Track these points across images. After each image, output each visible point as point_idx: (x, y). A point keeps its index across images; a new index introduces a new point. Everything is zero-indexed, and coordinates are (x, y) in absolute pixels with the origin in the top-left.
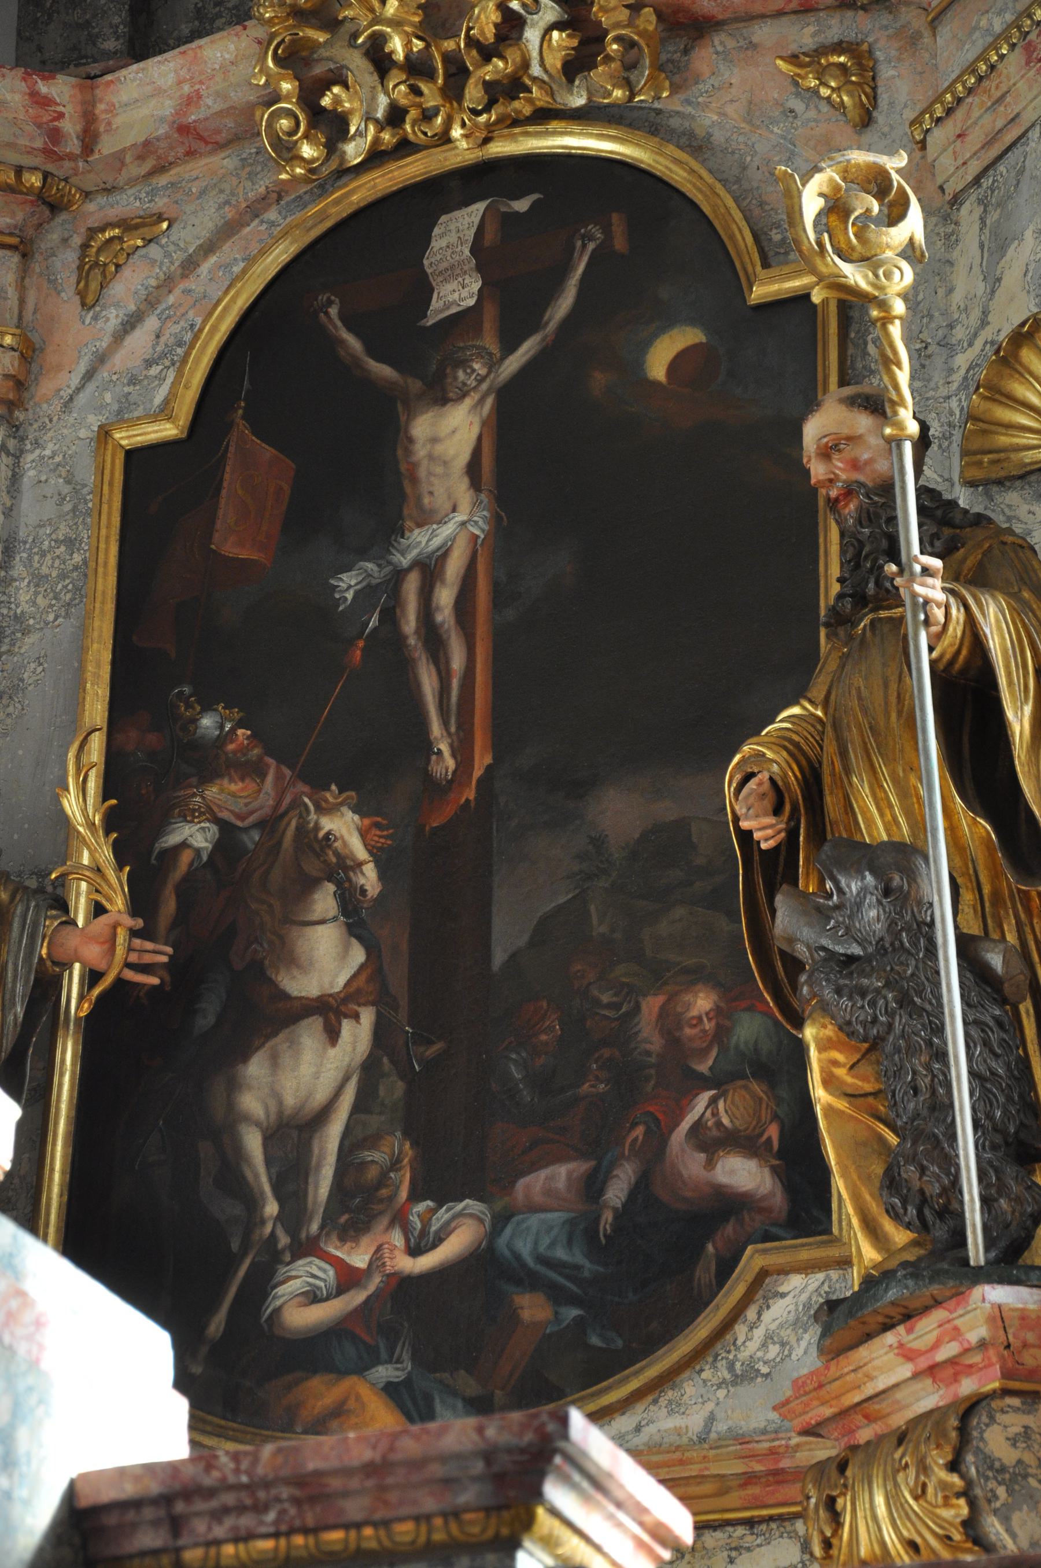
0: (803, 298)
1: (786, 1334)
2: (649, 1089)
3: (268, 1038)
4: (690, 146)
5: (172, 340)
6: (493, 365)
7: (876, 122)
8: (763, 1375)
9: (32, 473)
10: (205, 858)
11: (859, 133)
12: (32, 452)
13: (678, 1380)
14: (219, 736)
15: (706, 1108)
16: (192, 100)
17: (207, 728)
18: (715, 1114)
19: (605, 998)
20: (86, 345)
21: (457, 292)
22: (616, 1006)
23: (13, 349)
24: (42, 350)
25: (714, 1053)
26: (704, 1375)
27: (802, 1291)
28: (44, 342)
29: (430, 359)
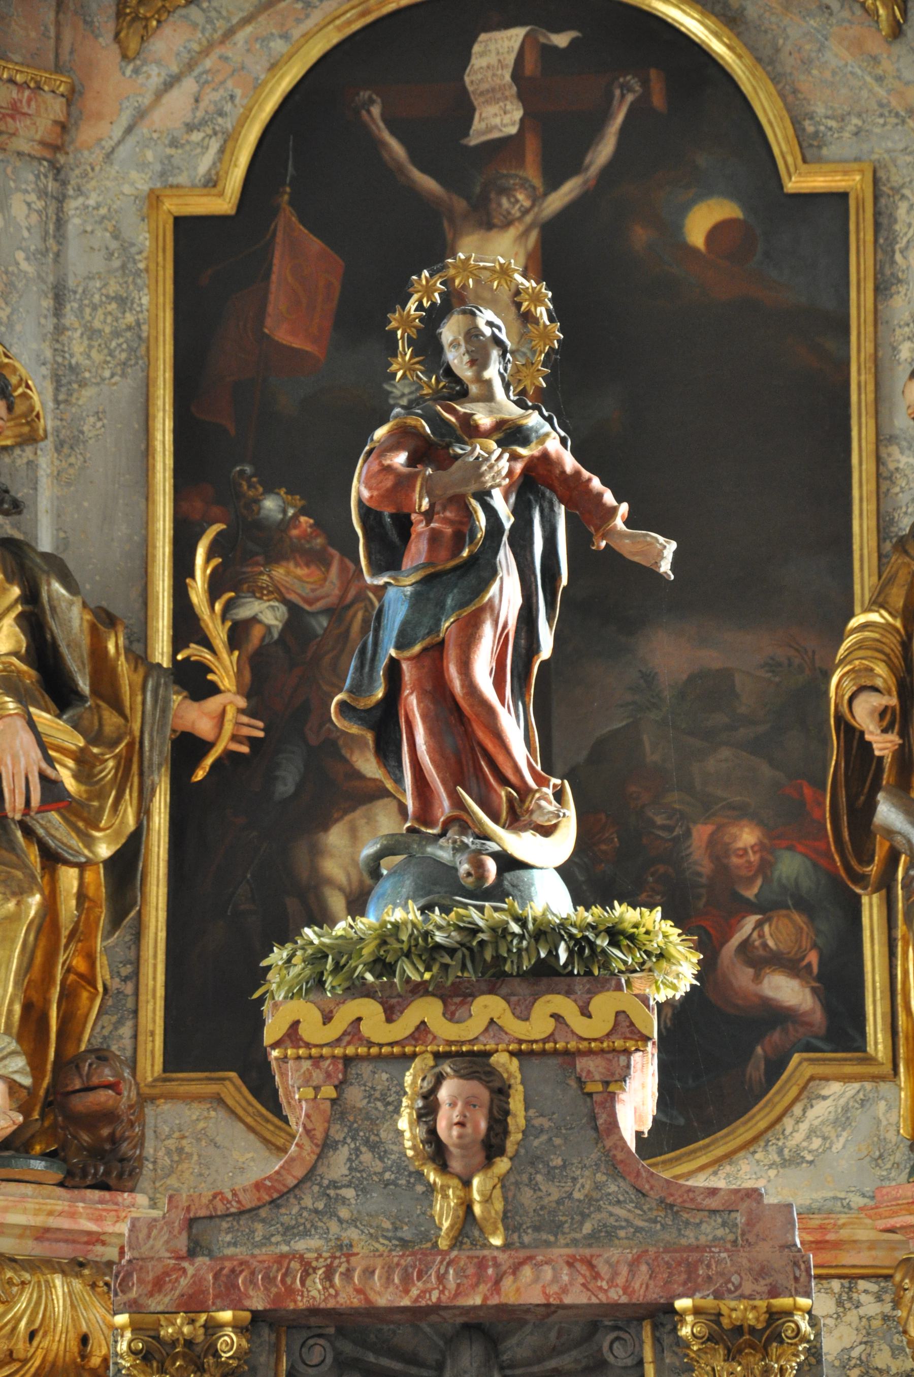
0: (843, 196)
1: (827, 1130)
2: (701, 904)
3: (346, 812)
4: (724, 15)
5: (212, 108)
6: (537, 199)
7: (905, 35)
8: (808, 1162)
9: (76, 221)
10: (276, 635)
11: (890, 43)
12: (76, 198)
13: (735, 1157)
14: (282, 520)
15: (754, 929)
17: (270, 510)
18: (761, 936)
19: (659, 820)
20: (127, 98)
21: (498, 118)
22: (670, 829)
23: (63, 95)
24: (81, 94)
25: (759, 882)
26: (757, 1156)
27: (841, 1096)
28: (83, 86)
29: (477, 179)
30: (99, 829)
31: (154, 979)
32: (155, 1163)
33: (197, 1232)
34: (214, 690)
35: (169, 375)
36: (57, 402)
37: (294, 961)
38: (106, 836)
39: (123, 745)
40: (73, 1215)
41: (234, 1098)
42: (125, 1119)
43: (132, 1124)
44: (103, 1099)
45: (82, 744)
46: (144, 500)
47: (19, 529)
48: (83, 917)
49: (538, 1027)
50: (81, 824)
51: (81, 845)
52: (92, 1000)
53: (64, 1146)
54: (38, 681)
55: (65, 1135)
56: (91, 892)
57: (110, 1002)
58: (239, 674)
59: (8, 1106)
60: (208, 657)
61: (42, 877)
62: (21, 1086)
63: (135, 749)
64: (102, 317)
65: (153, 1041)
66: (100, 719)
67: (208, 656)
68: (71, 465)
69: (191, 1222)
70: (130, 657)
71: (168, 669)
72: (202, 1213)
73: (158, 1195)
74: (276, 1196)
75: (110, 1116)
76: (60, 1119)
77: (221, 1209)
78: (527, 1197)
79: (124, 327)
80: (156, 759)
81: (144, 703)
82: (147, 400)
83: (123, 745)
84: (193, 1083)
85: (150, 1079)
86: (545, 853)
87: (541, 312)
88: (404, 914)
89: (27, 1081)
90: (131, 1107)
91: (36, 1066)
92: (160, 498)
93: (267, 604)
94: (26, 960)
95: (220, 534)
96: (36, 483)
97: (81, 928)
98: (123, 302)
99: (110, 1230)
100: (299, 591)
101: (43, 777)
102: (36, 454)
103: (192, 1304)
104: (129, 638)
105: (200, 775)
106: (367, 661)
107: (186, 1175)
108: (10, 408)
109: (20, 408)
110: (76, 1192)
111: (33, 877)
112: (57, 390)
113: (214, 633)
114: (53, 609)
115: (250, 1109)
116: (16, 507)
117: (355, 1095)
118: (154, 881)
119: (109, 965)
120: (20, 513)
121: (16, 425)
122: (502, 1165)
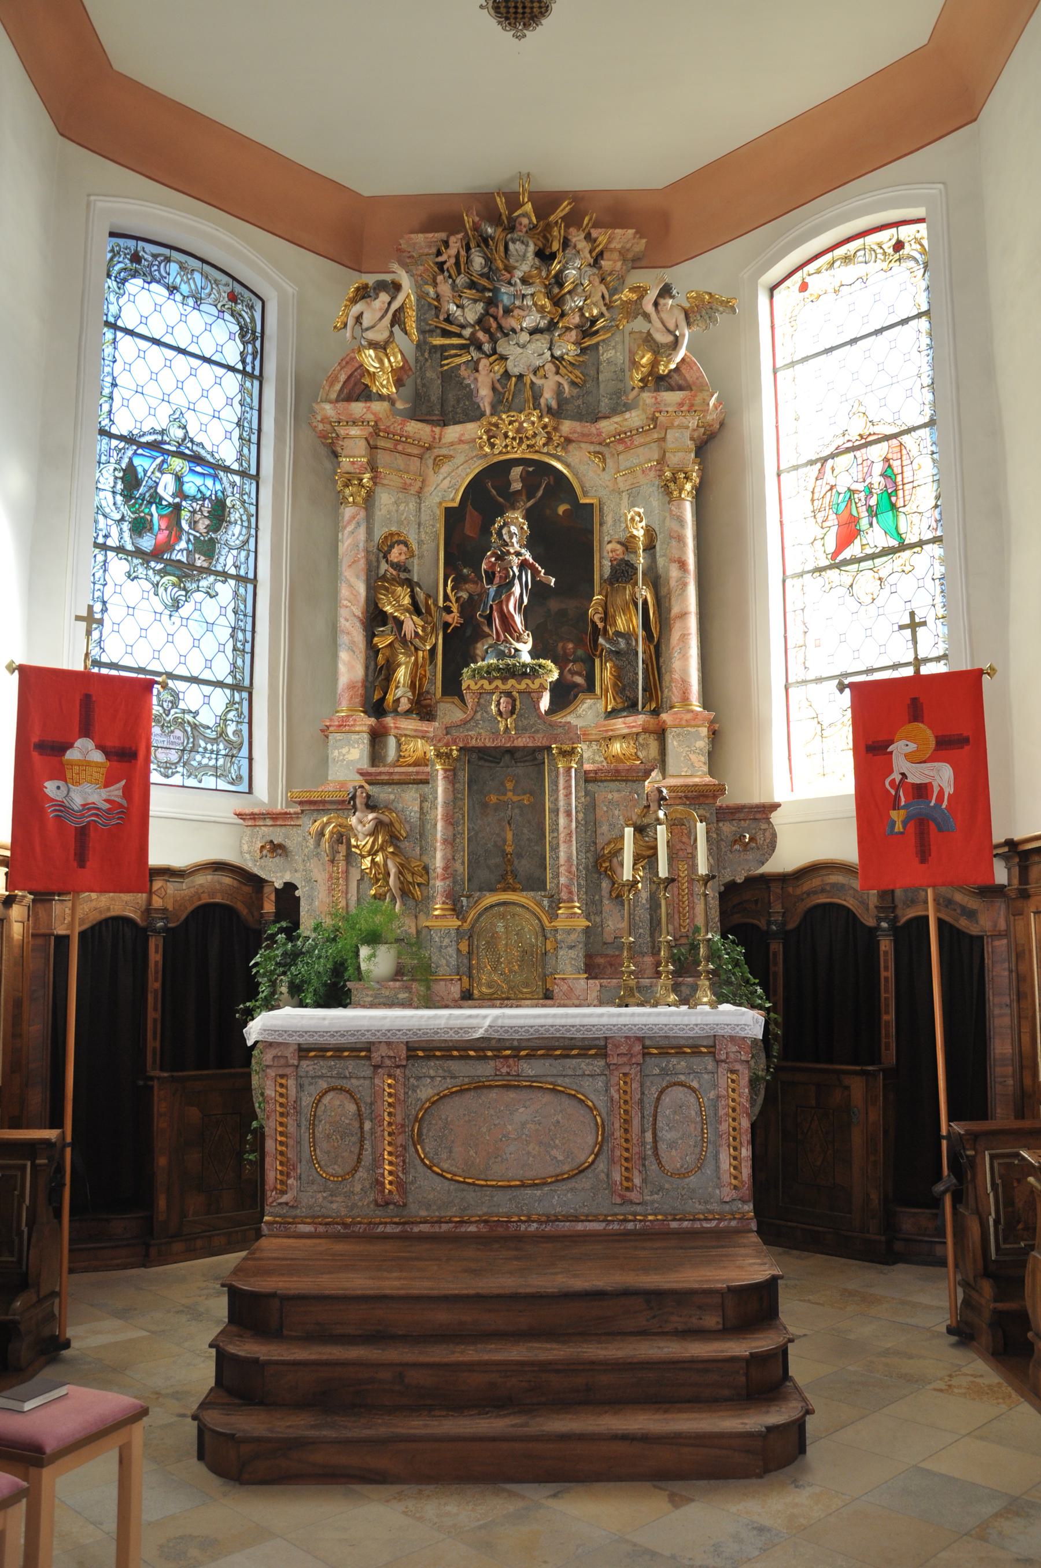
16: (463, 435)
21: (517, 486)
29: (511, 500)
33: (448, 730)
49: (522, 686)
74: (465, 723)
75: (430, 706)
78: (520, 723)
84: (448, 699)
86: (524, 649)
87: (525, 527)
88: (493, 661)
91: (414, 694)
98: (433, 526)
103: (447, 745)
106: (485, 605)
116: (409, 571)
117: (482, 701)
122: (515, 716)
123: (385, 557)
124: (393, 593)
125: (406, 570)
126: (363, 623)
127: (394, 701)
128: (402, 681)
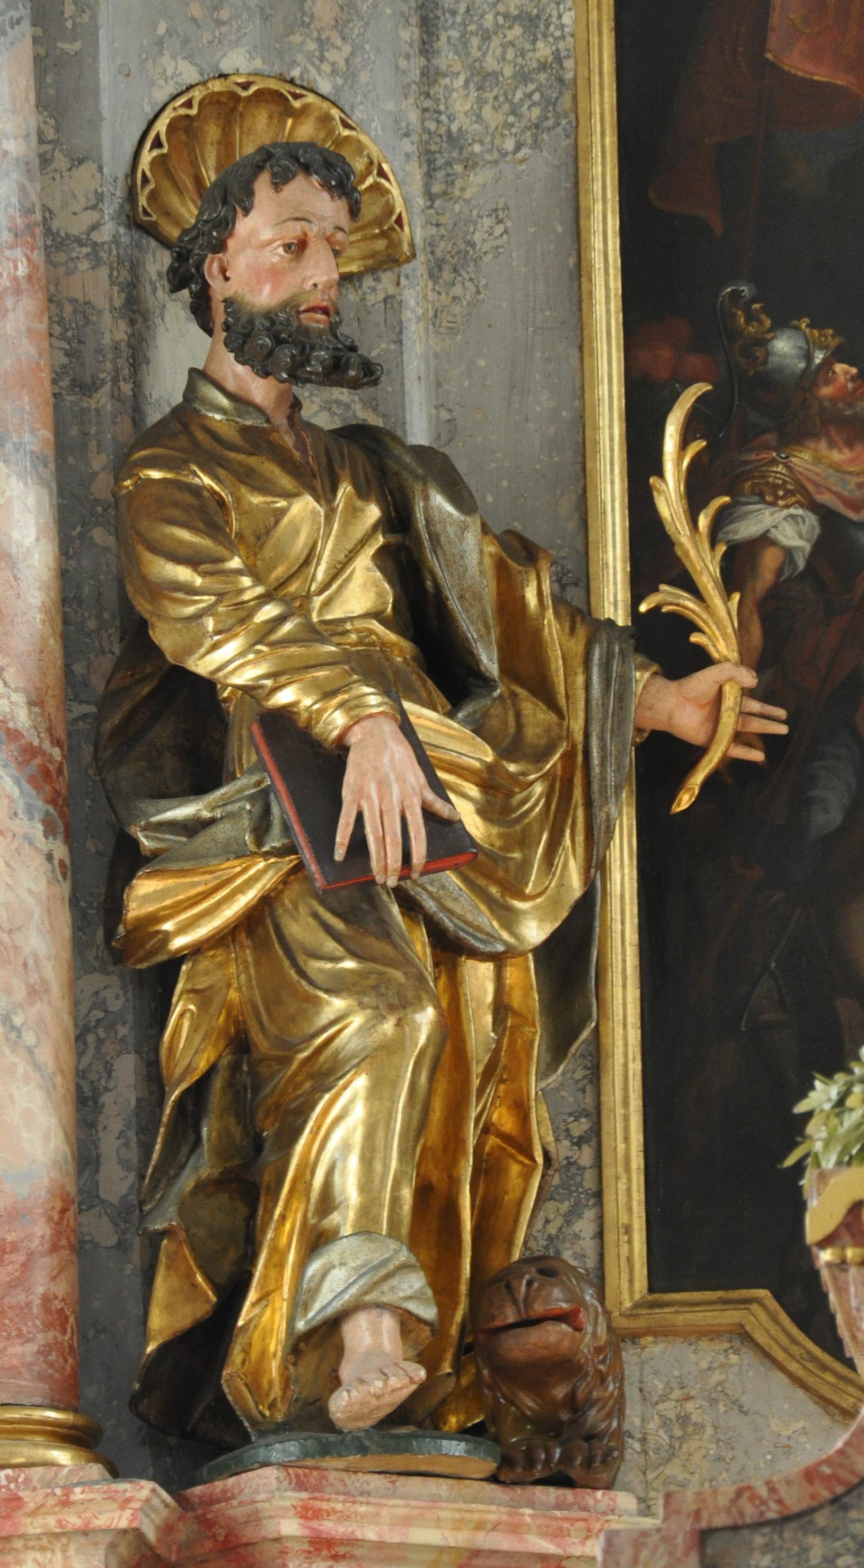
10: (801, 564)
14: (805, 371)
17: (785, 356)
30: (524, 897)
31: (626, 1139)
32: (643, 1440)
34: (701, 659)
35: (611, 140)
36: (430, 197)
37: (850, 1102)
38: (535, 908)
39: (557, 757)
40: (515, 1528)
41: (767, 1331)
42: (591, 1370)
43: (603, 1380)
44: (553, 1338)
45: (490, 757)
46: (576, 352)
47: (375, 409)
48: (505, 1041)
50: (494, 890)
51: (495, 924)
52: (527, 1177)
53: (494, 1416)
54: (414, 659)
55: (496, 1399)
56: (516, 1000)
57: (556, 1180)
58: (742, 631)
59: (401, 1356)
60: (691, 605)
61: (436, 979)
62: (419, 1320)
63: (578, 762)
64: (499, 52)
65: (630, 1242)
66: (518, 715)
67: (689, 603)
68: (455, 298)
69: (703, 1537)
70: (563, 611)
71: (625, 628)
72: (721, 1520)
73: (652, 1494)
75: (565, 1366)
76: (485, 1372)
77: (750, 1513)
79: (535, 65)
80: (611, 778)
81: (588, 686)
82: (576, 185)
83: (557, 757)
84: (697, 1308)
85: (628, 1304)
89: (429, 1312)
90: (598, 1350)
91: (443, 1289)
92: (601, 346)
93: (785, 512)
94: (416, 1114)
95: (702, 400)
96: (401, 332)
97: (503, 1060)
99: (577, 1551)
100: (838, 489)
101: (429, 815)
102: (398, 284)
104: (559, 580)
105: (685, 801)
107: (697, 1458)
108: (354, 211)
109: (370, 210)
110: (519, 1490)
111: (421, 979)
112: (429, 175)
113: (699, 566)
114: (435, 539)
115: (795, 1349)
116: (369, 374)
118: (618, 980)
119: (552, 1121)
120: (375, 383)
121: (364, 239)
123: (186, 275)
124: (258, 539)
125: (349, 367)
126: (43, 777)
127: (298, 1346)
128: (349, 1189)
